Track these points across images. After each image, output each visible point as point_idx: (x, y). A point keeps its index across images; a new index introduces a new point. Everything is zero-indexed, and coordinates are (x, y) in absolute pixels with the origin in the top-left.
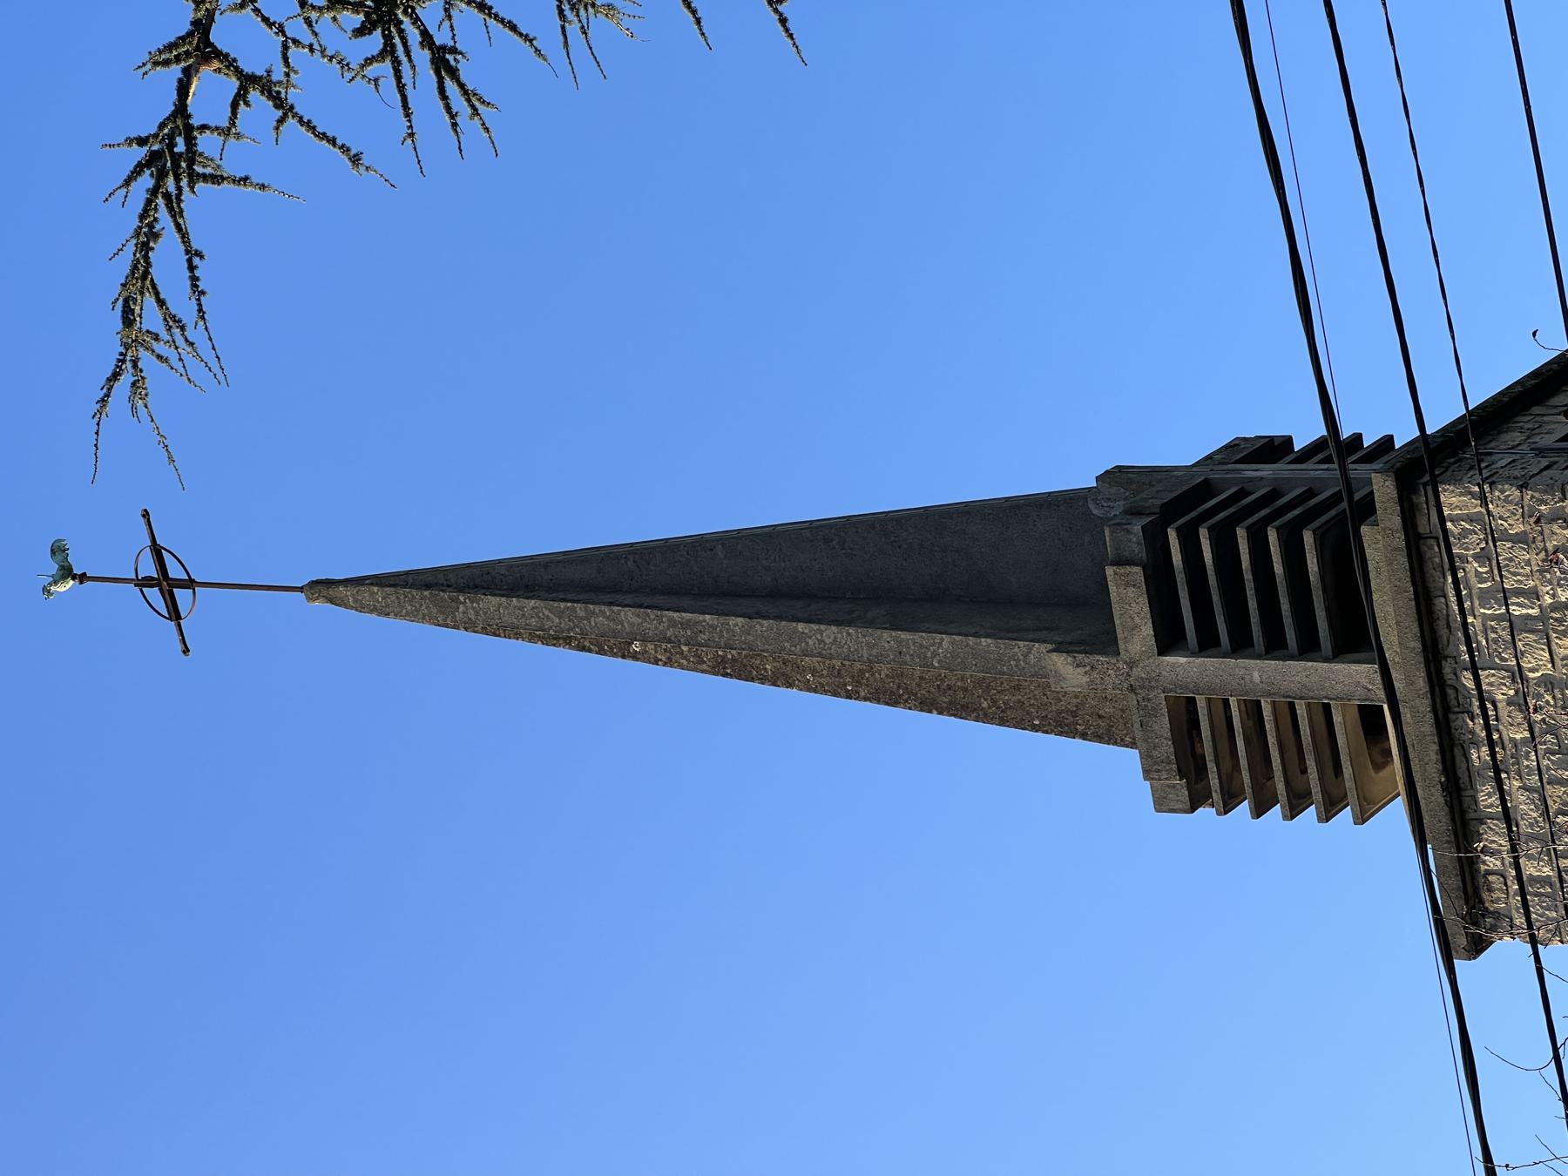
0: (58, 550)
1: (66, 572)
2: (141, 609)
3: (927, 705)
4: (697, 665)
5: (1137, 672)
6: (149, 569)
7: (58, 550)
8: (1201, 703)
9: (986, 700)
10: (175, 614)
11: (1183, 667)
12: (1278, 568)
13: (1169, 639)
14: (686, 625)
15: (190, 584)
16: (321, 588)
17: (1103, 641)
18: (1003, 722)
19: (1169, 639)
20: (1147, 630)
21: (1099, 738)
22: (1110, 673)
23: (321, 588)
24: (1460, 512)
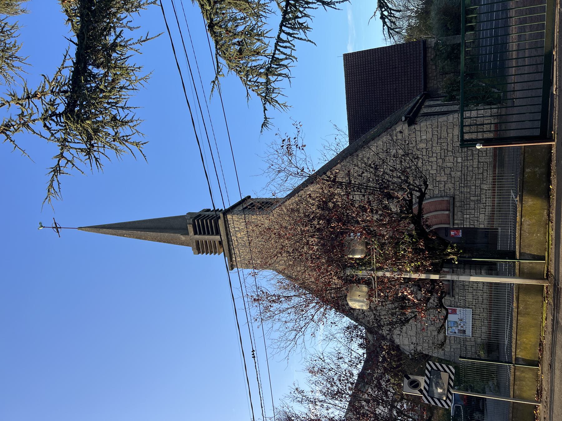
0: (40, 223)
1: (42, 226)
3: (164, 242)
7: (40, 223)
8: (199, 241)
10: (58, 232)
11: (197, 237)
12: (209, 225)
13: (195, 233)
14: (132, 232)
19: (195, 233)
21: (186, 246)
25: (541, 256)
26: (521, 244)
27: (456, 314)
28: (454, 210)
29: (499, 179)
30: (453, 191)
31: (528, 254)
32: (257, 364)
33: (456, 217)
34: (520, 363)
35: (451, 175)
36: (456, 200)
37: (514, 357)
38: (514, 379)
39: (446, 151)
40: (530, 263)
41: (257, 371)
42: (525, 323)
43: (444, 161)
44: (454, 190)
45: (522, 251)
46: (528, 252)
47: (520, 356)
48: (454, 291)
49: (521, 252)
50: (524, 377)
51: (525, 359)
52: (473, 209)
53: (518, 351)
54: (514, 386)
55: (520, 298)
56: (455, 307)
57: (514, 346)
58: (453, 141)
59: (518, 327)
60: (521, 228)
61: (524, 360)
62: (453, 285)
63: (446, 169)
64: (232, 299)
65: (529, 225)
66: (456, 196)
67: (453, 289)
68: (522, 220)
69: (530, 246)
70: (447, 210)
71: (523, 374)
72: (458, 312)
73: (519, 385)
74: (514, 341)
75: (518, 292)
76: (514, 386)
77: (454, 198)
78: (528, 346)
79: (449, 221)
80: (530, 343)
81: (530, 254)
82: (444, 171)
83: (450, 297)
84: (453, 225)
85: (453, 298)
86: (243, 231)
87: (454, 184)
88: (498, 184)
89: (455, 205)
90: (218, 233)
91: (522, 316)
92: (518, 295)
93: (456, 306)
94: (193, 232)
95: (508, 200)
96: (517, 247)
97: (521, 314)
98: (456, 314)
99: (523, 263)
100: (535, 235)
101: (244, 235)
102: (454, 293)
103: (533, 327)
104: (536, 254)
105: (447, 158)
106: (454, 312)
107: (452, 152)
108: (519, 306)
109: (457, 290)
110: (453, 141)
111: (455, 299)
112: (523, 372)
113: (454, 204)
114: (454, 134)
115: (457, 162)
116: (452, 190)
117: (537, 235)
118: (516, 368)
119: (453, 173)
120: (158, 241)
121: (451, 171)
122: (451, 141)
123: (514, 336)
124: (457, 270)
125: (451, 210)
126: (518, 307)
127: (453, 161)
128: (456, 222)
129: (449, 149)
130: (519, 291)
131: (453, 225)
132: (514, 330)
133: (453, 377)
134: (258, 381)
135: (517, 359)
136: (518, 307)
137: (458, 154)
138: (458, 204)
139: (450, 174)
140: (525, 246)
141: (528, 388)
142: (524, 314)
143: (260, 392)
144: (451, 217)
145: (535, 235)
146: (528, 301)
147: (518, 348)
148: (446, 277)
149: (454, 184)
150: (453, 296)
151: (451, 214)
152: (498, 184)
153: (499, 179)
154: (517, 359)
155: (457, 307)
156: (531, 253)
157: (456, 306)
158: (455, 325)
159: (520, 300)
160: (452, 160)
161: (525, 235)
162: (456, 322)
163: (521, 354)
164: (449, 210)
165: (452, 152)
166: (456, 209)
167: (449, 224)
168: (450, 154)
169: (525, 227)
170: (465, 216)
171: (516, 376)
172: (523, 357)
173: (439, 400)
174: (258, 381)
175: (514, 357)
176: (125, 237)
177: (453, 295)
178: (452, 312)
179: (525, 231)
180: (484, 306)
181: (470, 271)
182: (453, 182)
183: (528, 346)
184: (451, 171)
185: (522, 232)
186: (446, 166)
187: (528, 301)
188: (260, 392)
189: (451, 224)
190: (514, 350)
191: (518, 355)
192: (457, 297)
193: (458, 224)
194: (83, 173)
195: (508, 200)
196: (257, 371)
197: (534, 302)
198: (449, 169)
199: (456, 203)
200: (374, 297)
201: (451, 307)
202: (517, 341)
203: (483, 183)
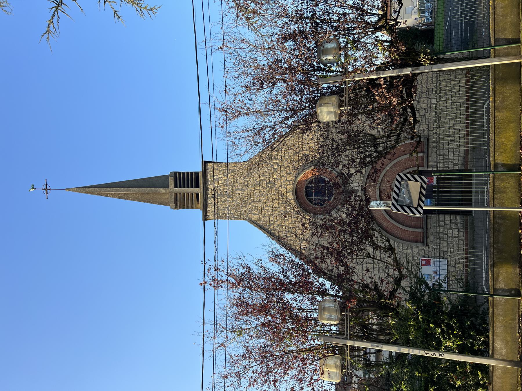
0: (33, 185)
1: (33, 188)
2: (42, 193)
3: (144, 202)
4: (116, 197)
5: (171, 190)
6: (45, 187)
7: (33, 185)
8: (178, 195)
9: (374, 229)
10: (47, 193)
11: (177, 190)
12: (190, 177)
13: (176, 186)
14: (116, 189)
15: (50, 189)
16: (85, 189)
17: (168, 187)
18: (154, 203)
19: (176, 186)
20: (173, 185)
21: (165, 205)
22: (168, 190)
23: (85, 189)
24: (404, 143)
25: (515, 39)
26: (495, 29)
27: (430, 266)
28: (428, 151)
29: (473, 125)
30: (427, 132)
31: (502, 39)
32: (216, 253)
33: (430, 158)
34: (500, 170)
35: (425, 116)
36: (430, 141)
37: (492, 163)
38: (494, 191)
39: (421, 93)
40: (505, 49)
41: (215, 247)
42: (503, 119)
43: (419, 103)
44: (428, 131)
45: (496, 37)
46: (503, 37)
47: (499, 162)
48: (428, 239)
49: (496, 37)
50: (505, 187)
51: (505, 164)
52: (446, 241)
53: (497, 154)
54: (494, 200)
55: (496, 90)
56: (429, 257)
57: (492, 149)
58: (427, 83)
59: (496, 125)
60: (494, 11)
61: (503, 165)
62: (427, 233)
63: (420, 110)
64: (202, 354)
65: (502, 8)
66: (430, 137)
67: (427, 237)
68: (495, 4)
69: (504, 29)
70: (420, 228)
71: (503, 184)
72: (432, 264)
73: (500, 198)
74: (492, 144)
75: (495, 84)
76: (494, 200)
77: (428, 139)
78: (508, 148)
79: (423, 163)
80: (510, 143)
81: (505, 39)
82: (419, 112)
83: (424, 245)
84: (427, 168)
85: (427, 247)
86: (222, 180)
87: (428, 125)
88: (471, 125)
89: (429, 146)
90: (197, 186)
91: (499, 112)
92: (495, 87)
93: (430, 256)
94: (173, 185)
95: (482, 119)
96: (492, 33)
97: (498, 109)
98: (430, 266)
99: (498, 50)
100: (508, 17)
101: (222, 183)
102: (428, 241)
103: (512, 122)
104: (510, 37)
105: (422, 99)
106: (428, 263)
107: (427, 94)
108: (496, 100)
109: (431, 238)
110: (427, 83)
111: (429, 248)
112: (503, 181)
113: (428, 145)
114: (428, 77)
115: (431, 103)
116: (426, 131)
117: (510, 17)
118: (496, 176)
119: (427, 114)
120: (138, 201)
121: (425, 112)
122: (426, 84)
123: (491, 135)
124: (431, 216)
125: (426, 150)
126: (495, 101)
127: (427, 103)
128: (430, 164)
129: (424, 91)
130: (495, 82)
131: (427, 168)
132: (492, 129)
133: (424, 192)
134: (215, 226)
135: (496, 165)
136: (495, 101)
137: (432, 96)
138: (432, 145)
139: (424, 115)
140: (499, 30)
141: (510, 201)
142: (502, 109)
143: (215, 241)
144: (425, 159)
145: (508, 17)
146: (505, 93)
147: (497, 152)
148: (419, 69)
149: (428, 125)
150: (427, 245)
151: (425, 155)
152: (471, 125)
153: (473, 125)
154: (496, 165)
155: (431, 258)
156: (506, 37)
157: (430, 256)
158: (429, 279)
159: (496, 92)
160: (426, 101)
161: (499, 18)
162: (430, 275)
163: (501, 159)
164: (424, 152)
165: (427, 94)
166: (430, 150)
167: (423, 167)
168: (424, 95)
169: (499, 10)
170: (438, 247)
171: (495, 187)
172: (503, 162)
173: (409, 208)
174: (215, 226)
175: (492, 163)
176: (108, 196)
177: (427, 244)
178: (426, 264)
179: (499, 15)
180: (459, 256)
181: (445, 217)
182: (427, 123)
183: (508, 148)
184: (425, 112)
185: (495, 16)
186: (421, 107)
187: (505, 93)
188: (215, 241)
189: (426, 166)
190: (492, 154)
191: (497, 160)
192: (431, 246)
193: (432, 166)
194: (82, 10)
195: (482, 119)
196: (215, 247)
197: (511, 93)
198: (424, 110)
199: (430, 144)
200: (346, 369)
201: (425, 257)
202: (496, 143)
203: (456, 124)
